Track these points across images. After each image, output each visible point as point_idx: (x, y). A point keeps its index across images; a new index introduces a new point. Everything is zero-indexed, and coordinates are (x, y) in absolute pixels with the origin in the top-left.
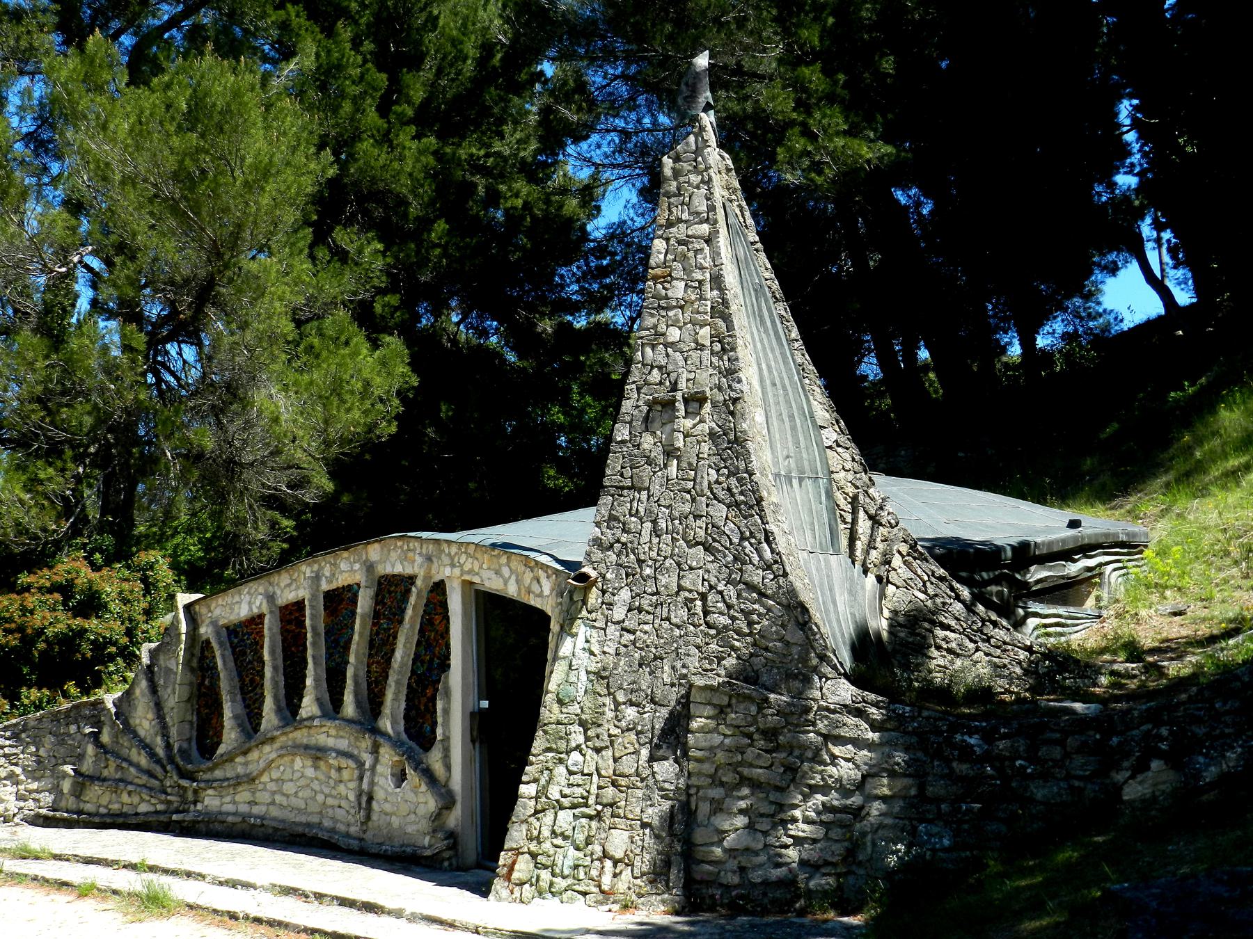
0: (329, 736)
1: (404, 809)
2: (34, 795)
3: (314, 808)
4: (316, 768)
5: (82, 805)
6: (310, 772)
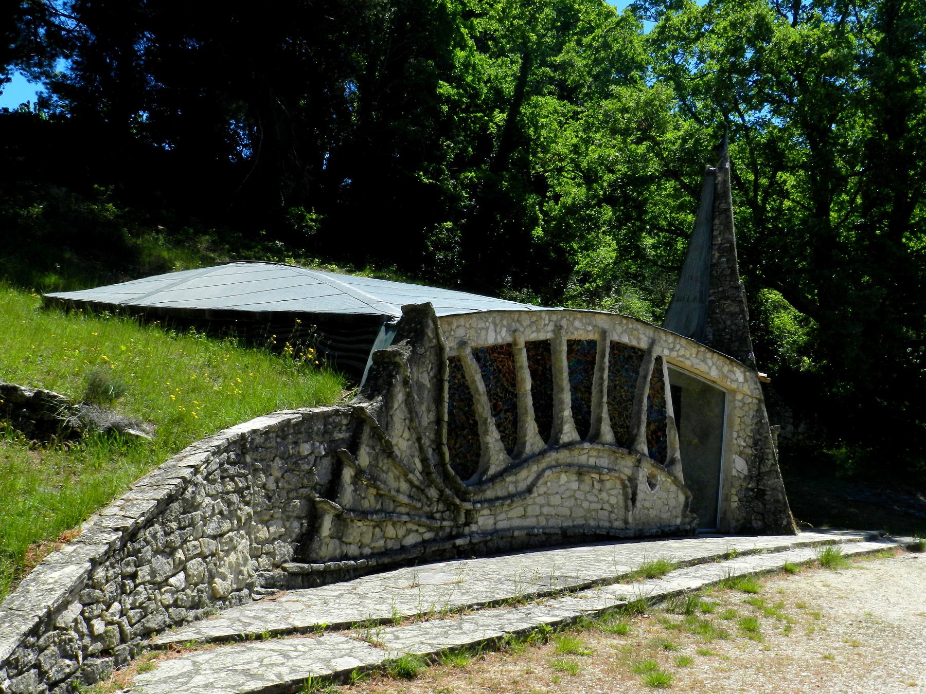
0: (588, 455)
1: (659, 504)
2: (268, 547)
3: (579, 513)
4: (580, 481)
5: (345, 549)
6: (575, 485)
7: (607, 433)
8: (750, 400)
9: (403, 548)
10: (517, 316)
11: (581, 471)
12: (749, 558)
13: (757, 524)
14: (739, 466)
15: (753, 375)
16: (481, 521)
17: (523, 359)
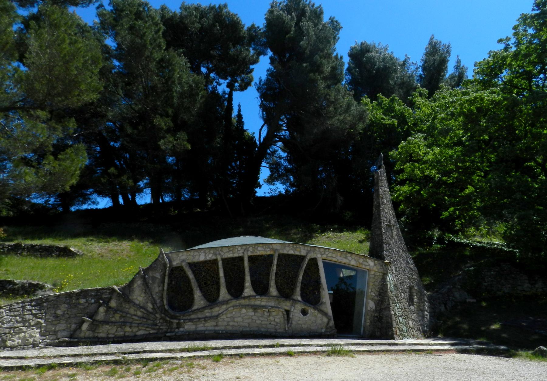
7: (273, 291)
8: (379, 274)
9: (136, 336)
10: (220, 249)
11: (255, 308)
12: (73, 353)
13: (378, 334)
14: (372, 305)
15: (380, 262)
16: (186, 327)
17: (220, 264)
